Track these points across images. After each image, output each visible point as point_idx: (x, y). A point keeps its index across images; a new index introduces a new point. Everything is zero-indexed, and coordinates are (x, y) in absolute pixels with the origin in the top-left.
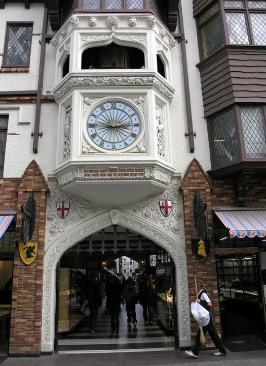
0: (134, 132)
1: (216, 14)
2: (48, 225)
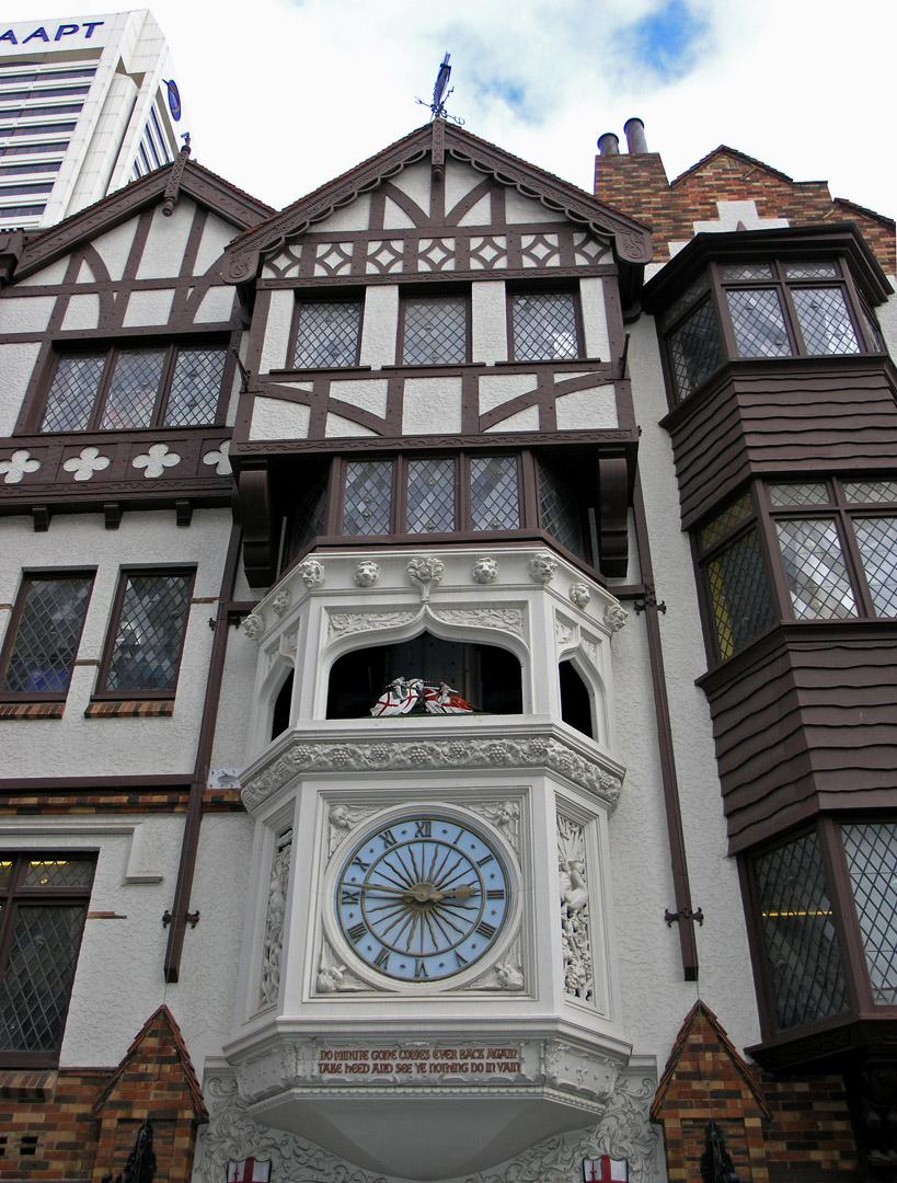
0: (486, 918)
1: (748, 525)
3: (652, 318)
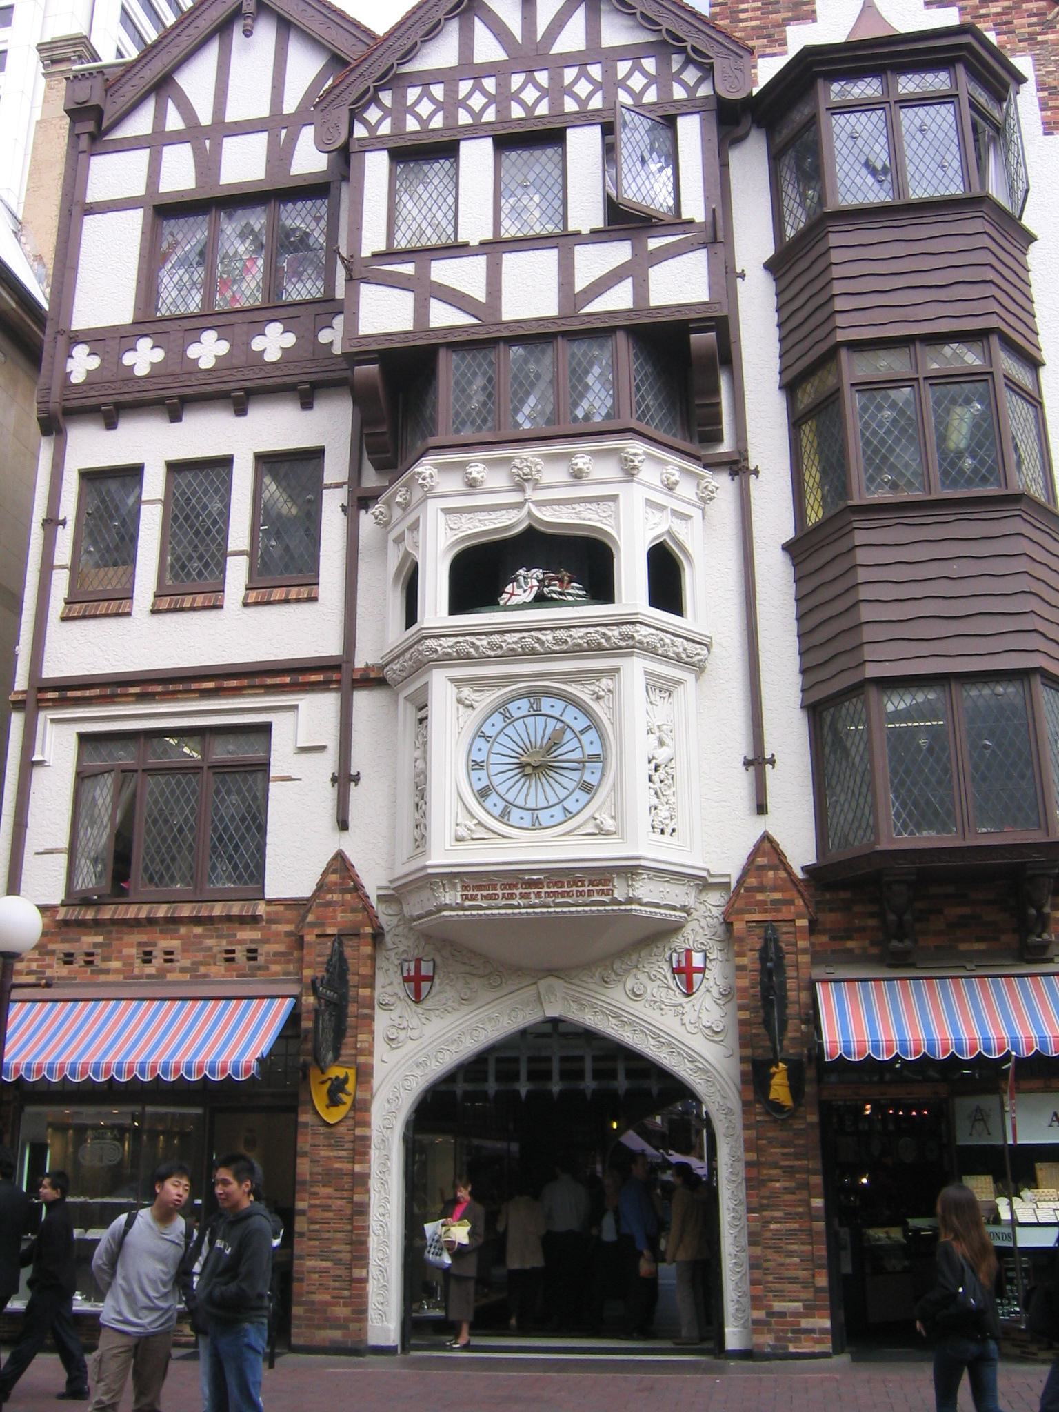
2: (382, 1021)
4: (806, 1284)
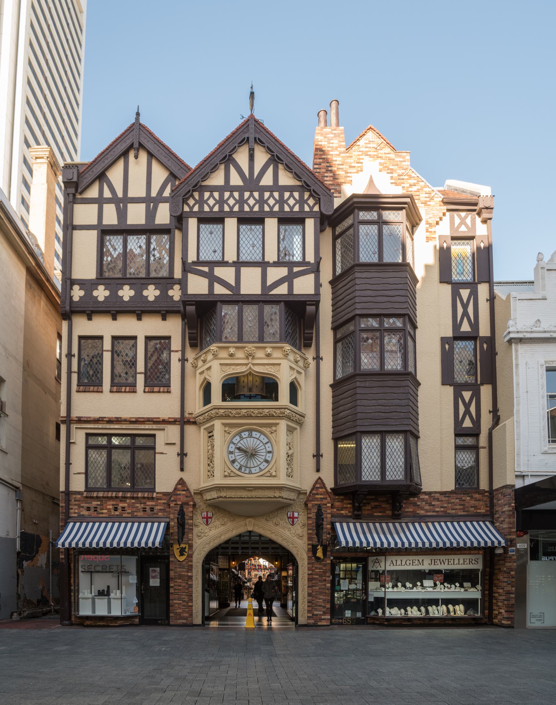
0: (267, 458)
3: (331, 228)
4: (324, 607)
